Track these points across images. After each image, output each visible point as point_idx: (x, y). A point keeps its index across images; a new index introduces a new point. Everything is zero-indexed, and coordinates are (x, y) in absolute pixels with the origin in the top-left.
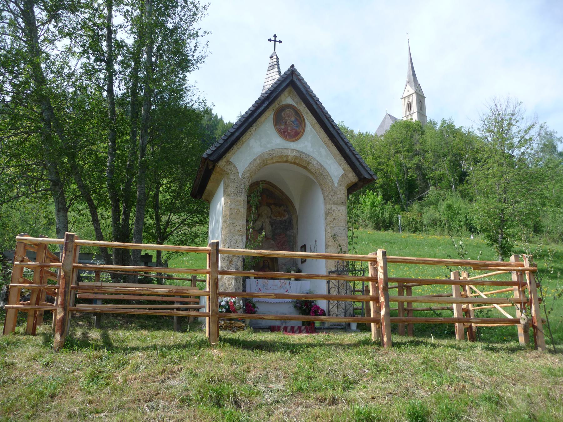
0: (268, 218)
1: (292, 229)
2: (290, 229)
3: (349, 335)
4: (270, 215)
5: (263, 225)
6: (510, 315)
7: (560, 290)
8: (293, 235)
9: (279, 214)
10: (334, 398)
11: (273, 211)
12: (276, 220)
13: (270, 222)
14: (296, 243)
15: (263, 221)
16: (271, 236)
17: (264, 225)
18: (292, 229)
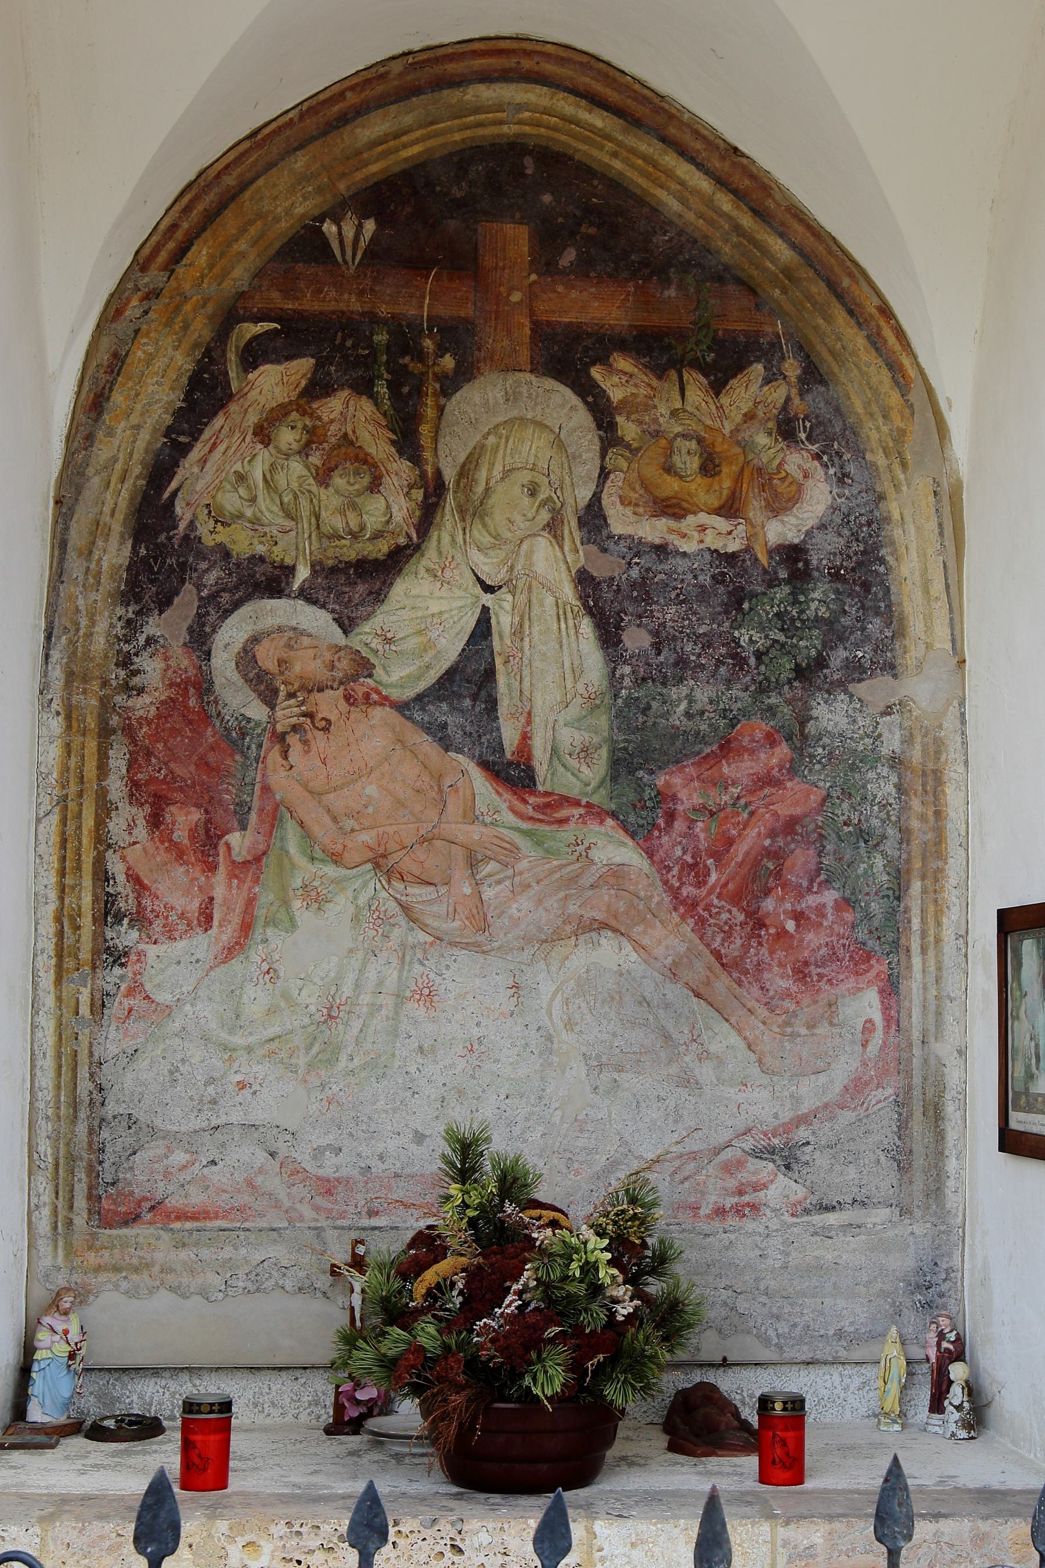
0: (553, 527)
1: (891, 668)
2: (856, 671)
3: (253, 261)
4: (585, 494)
5: (483, 628)
6: (826, 1491)
7: (310, 1560)
8: (892, 742)
9: (709, 467)
10: (823, 382)
11: (628, 428)
12: (661, 550)
13: (584, 580)
14: (937, 847)
15: (490, 569)
16: (595, 771)
17: (503, 621)
18: (891, 668)
